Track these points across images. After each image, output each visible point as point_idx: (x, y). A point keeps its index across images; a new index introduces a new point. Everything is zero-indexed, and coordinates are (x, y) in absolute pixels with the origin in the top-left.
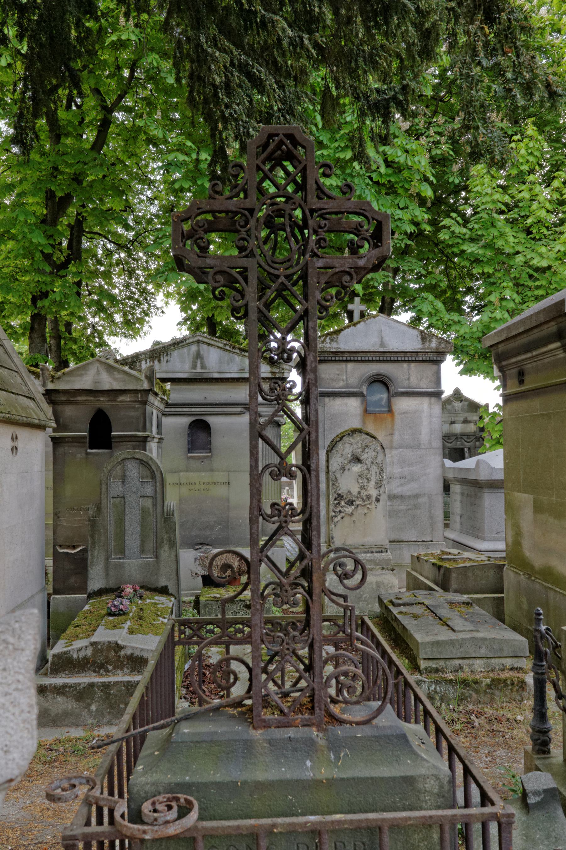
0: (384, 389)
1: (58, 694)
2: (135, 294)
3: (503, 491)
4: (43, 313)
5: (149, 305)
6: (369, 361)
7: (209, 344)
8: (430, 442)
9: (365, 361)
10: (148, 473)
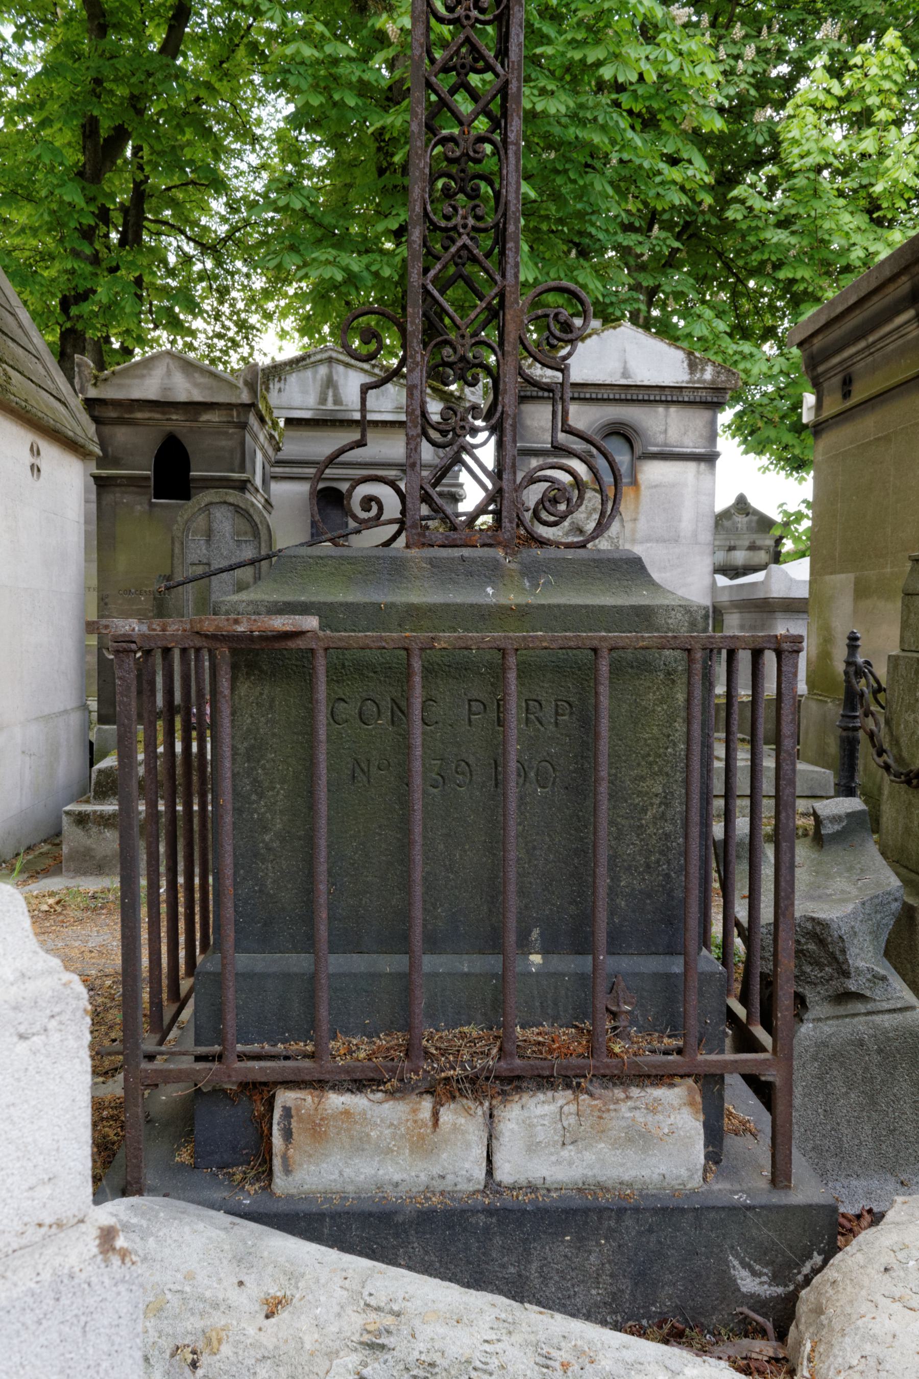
0: (626, 447)
1: (106, 826)
2: (229, 329)
3: (805, 616)
4: (79, 327)
5: (252, 348)
6: (603, 400)
7: (347, 365)
8: (695, 534)
9: (597, 400)
10: (248, 528)
